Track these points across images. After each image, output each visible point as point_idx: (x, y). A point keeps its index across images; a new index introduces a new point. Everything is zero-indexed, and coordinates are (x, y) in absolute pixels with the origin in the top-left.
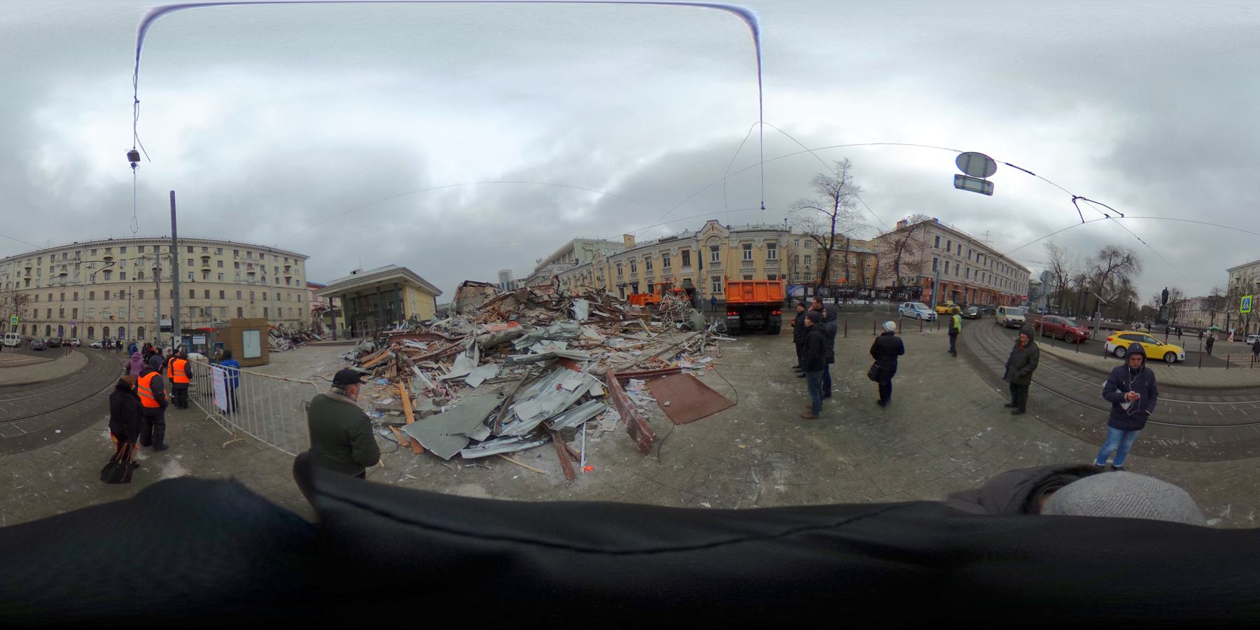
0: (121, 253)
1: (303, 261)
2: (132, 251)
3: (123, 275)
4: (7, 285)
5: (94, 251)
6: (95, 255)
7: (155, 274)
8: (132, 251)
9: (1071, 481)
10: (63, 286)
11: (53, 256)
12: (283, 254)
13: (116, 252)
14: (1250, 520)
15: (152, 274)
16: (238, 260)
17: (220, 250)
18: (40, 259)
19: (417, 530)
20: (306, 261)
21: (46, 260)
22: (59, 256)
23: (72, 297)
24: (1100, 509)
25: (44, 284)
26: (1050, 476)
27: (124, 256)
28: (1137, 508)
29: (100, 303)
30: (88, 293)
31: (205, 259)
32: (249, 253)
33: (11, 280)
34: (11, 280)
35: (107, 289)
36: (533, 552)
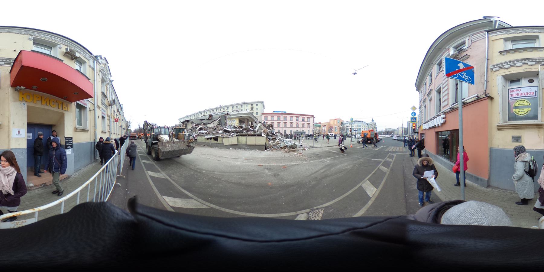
0: (256, 106)
6: (242, 107)
11: (233, 107)
12: (214, 109)
19: (173, 229)
24: (461, 216)
28: (476, 215)
32: (237, 107)
36: (222, 240)
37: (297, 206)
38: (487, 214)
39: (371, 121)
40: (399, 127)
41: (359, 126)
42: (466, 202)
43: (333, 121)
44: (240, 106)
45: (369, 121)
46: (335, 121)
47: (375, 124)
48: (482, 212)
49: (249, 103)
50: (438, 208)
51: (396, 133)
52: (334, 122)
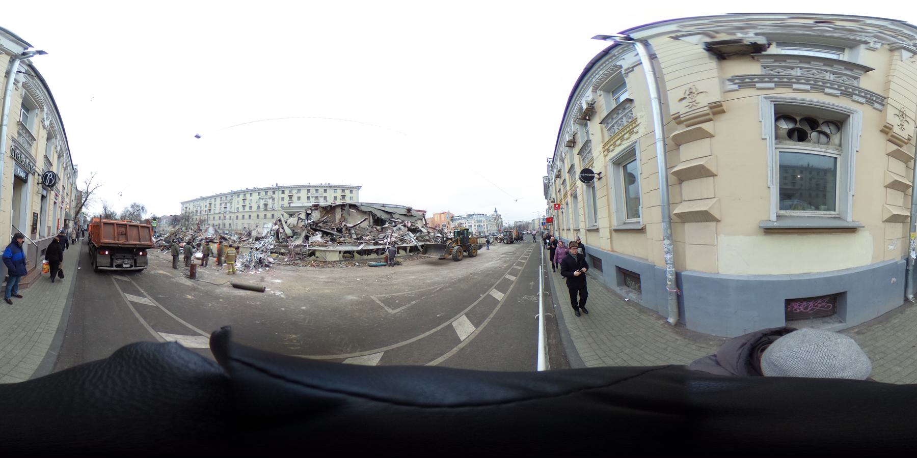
1: (358, 190)
2: (255, 195)
3: (251, 207)
4: (201, 212)
5: (238, 196)
7: (265, 206)
8: (255, 195)
9: (768, 346)
10: (225, 213)
13: (248, 196)
14: (916, 382)
15: (263, 207)
16: (310, 195)
17: (299, 191)
18: (215, 199)
20: (360, 190)
21: (218, 200)
22: (224, 198)
23: (229, 218)
25: (217, 212)
26: (761, 338)
27: (251, 198)
29: (246, 221)
30: (235, 217)
31: (291, 197)
33: (202, 209)
34: (202, 209)
35: (250, 214)
37: (365, 344)
38: (835, 350)
39: (494, 213)
40: (535, 218)
41: (479, 222)
42: (795, 332)
43: (439, 216)
44: (323, 191)
45: (490, 212)
46: (443, 215)
47: (499, 217)
48: (828, 348)
49: (339, 187)
50: (751, 344)
51: (531, 227)
52: (440, 217)
